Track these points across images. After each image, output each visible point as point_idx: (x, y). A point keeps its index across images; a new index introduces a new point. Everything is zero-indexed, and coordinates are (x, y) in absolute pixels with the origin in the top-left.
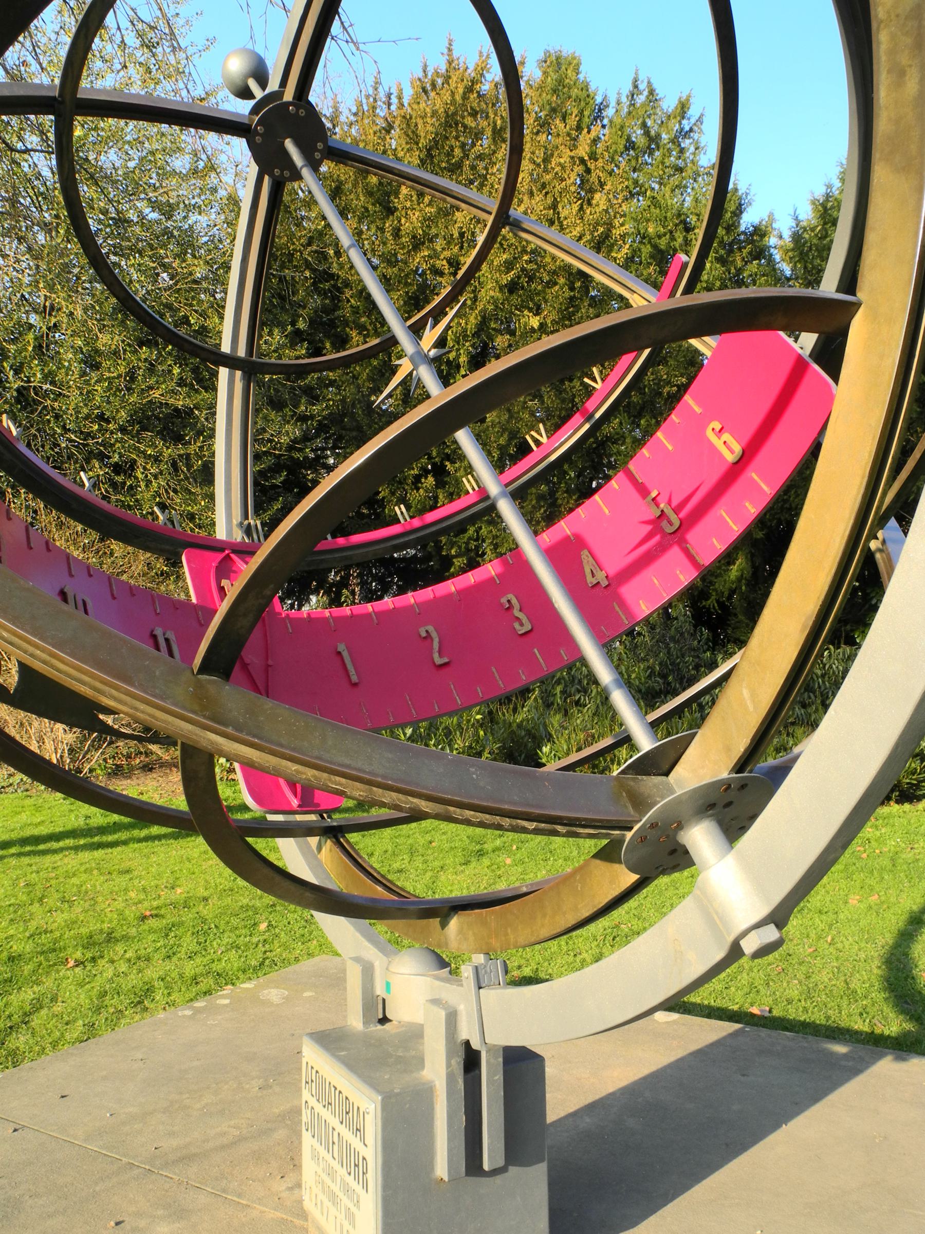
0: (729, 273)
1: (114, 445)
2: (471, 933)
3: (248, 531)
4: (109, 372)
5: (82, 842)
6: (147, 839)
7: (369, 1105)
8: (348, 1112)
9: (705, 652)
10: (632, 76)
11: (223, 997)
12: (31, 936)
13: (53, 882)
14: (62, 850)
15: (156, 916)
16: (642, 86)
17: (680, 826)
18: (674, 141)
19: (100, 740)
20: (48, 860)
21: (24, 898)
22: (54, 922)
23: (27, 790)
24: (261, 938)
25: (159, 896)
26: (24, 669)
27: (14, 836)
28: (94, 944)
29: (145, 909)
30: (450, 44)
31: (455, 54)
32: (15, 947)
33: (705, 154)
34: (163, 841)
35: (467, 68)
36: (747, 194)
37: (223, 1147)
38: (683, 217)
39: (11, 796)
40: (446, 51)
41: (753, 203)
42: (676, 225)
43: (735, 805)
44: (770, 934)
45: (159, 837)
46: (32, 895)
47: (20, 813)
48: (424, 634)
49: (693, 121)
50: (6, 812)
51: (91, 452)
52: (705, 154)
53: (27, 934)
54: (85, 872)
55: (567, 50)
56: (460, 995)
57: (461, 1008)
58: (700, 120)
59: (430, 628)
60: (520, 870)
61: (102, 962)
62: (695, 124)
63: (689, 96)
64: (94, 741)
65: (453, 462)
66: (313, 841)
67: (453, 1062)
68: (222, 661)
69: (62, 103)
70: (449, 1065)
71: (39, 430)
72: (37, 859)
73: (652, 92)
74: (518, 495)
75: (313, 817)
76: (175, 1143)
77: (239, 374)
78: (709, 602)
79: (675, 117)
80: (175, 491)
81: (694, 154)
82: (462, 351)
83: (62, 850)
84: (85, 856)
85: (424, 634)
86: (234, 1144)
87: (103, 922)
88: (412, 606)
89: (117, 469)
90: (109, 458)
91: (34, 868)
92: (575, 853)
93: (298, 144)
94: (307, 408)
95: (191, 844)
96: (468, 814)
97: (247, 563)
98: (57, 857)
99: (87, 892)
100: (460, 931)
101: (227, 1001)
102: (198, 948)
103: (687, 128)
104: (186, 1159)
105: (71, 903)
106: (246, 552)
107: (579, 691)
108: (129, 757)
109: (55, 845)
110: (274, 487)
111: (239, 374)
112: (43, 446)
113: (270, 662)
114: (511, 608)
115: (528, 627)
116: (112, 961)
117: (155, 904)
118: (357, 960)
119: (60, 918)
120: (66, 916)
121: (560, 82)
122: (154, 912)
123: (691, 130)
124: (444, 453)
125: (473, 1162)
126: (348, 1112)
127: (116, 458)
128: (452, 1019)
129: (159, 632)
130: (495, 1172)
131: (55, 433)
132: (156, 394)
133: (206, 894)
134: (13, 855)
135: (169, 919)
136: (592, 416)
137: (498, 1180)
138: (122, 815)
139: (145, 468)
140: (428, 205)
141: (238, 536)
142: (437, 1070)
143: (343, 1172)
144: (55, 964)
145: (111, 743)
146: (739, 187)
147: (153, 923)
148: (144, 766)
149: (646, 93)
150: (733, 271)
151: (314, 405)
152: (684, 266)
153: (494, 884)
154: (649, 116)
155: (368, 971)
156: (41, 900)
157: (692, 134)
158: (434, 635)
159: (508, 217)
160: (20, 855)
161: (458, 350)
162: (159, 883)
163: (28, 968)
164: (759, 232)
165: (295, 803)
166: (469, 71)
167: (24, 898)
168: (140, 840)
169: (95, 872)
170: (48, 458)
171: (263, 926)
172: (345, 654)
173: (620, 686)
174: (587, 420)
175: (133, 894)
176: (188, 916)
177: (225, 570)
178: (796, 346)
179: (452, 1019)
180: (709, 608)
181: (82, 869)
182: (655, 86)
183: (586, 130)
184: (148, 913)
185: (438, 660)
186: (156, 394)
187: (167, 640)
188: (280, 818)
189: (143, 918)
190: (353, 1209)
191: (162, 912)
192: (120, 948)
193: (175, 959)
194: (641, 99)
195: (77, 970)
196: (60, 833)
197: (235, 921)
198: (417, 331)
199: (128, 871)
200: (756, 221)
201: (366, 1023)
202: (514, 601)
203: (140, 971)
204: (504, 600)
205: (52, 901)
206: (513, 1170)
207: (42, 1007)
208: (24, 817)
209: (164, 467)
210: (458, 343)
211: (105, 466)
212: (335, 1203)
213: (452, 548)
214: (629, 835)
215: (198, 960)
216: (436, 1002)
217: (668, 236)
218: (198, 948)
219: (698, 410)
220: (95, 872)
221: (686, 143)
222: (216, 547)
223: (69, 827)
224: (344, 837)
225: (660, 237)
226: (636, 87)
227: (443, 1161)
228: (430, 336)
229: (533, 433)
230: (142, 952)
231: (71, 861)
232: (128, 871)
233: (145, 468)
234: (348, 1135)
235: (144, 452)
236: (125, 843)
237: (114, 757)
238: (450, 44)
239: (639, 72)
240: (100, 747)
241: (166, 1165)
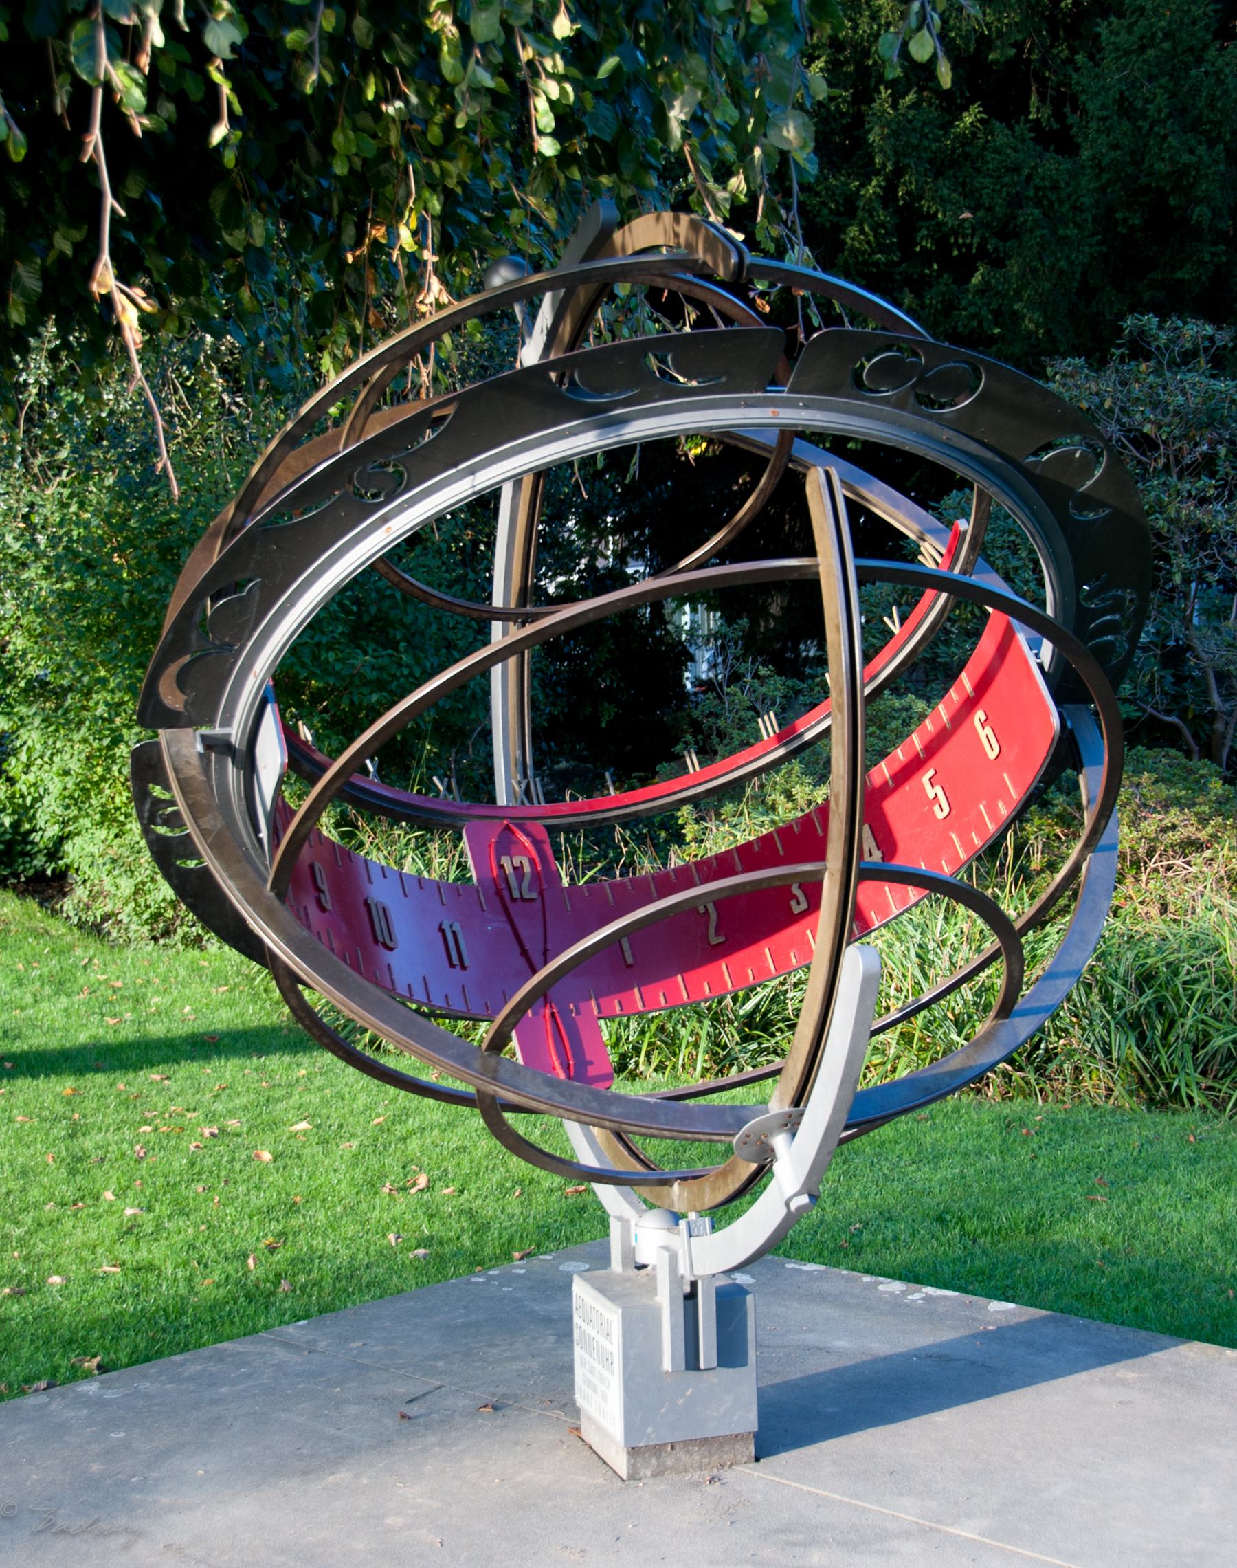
2: (42, 547)
8: (602, 1325)
43: (791, 1124)
44: (804, 1199)
56: (678, 1240)
57: (680, 1253)
118: (619, 1219)
125: (692, 1362)
128: (673, 1259)
129: (446, 926)
138: (707, 1106)
142: (665, 1301)
164: (1199, 223)
179: (673, 1259)
185: (714, 940)
187: (454, 933)
201: (624, 1266)
216: (666, 1248)
224: (463, 877)
227: (668, 1355)
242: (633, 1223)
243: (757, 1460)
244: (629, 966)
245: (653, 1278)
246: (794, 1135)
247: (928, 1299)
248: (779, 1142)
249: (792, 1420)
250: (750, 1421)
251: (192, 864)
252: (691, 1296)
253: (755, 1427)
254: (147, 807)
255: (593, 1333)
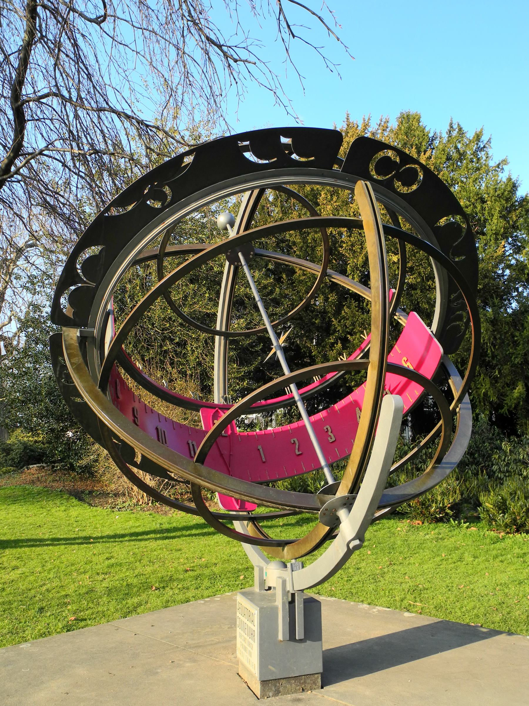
0: (509, 224)
1: (176, 333)
3: (226, 399)
4: (175, 297)
5: (158, 536)
6: (189, 535)
7: (255, 611)
8: (250, 616)
9: (497, 440)
10: (450, 121)
11: (217, 597)
12: (136, 576)
13: (145, 553)
14: (149, 539)
15: (192, 570)
16: (455, 126)
17: (336, 511)
18: (475, 154)
19: (167, 485)
20: (143, 543)
21: (133, 559)
22: (146, 570)
23: (132, 510)
24: (240, 583)
25: (194, 562)
26: (143, 456)
27: (127, 532)
28: (164, 581)
29: (187, 567)
30: (348, 116)
31: (351, 120)
32: (129, 580)
33: (492, 160)
34: (197, 537)
35: (358, 126)
36: (517, 181)
37: (211, 644)
38: (480, 196)
39: (124, 513)
40: (345, 120)
41: (521, 185)
42: (476, 200)
43: (348, 503)
44: (357, 542)
45: (195, 535)
46: (136, 558)
47: (129, 521)
48: (293, 442)
49: (485, 142)
50: (122, 520)
51: (165, 337)
52: (492, 160)
53: (134, 575)
54: (160, 549)
55: (413, 111)
56: (286, 574)
57: (287, 579)
58: (489, 141)
59: (295, 439)
60: (374, 557)
61: (167, 589)
62: (486, 144)
63: (482, 129)
64: (164, 485)
65: (351, 335)
66: (245, 522)
67: (285, 598)
68: (201, 459)
69: (160, 255)
70: (283, 599)
71: (141, 327)
72: (138, 543)
73: (460, 129)
74: (304, 399)
75: (245, 513)
76: (194, 642)
77: (223, 337)
78: (503, 410)
79: (473, 142)
80: (206, 355)
81: (486, 160)
82: (355, 276)
83: (149, 539)
84: (160, 542)
85: (293, 442)
86: (216, 643)
87: (168, 572)
88: (289, 430)
89: (178, 344)
90: (174, 340)
91: (136, 546)
92: (406, 550)
93: (243, 255)
94: (273, 310)
95: (210, 539)
96: (269, 504)
97: (224, 413)
98: (147, 542)
99: (161, 559)
100: (288, 552)
101: (219, 599)
102: (211, 585)
103: (482, 146)
104: (198, 646)
105: (153, 563)
106: (225, 408)
107: (421, 462)
108: (181, 494)
109: (146, 537)
110: (256, 351)
111: (223, 337)
112: (142, 334)
113: (231, 453)
114: (327, 431)
115: (334, 439)
116: (172, 589)
117: (192, 565)
118: (258, 566)
119: (149, 569)
120: (151, 568)
121: (409, 128)
122: (191, 569)
123: (484, 147)
124: (346, 332)
125: (292, 636)
126: (250, 616)
127: (177, 340)
128: (284, 583)
129: (190, 442)
130: (301, 641)
131: (148, 328)
132: (197, 307)
133: (216, 562)
134: (126, 541)
135: (198, 572)
136: (364, 350)
137: (303, 645)
139: (191, 345)
140: (335, 202)
141: (222, 402)
142: (279, 602)
143: (248, 638)
144: (147, 589)
145: (173, 486)
146: (512, 177)
147: (191, 573)
148: (189, 499)
149: (457, 130)
150: (511, 222)
151: (277, 308)
152: (394, 294)
153: (359, 563)
154: (460, 142)
155: (261, 570)
156: (140, 561)
157: (485, 149)
158: (297, 442)
159: (326, 273)
160: (129, 541)
161: (353, 275)
162: (194, 556)
163: (135, 590)
165: (238, 507)
166: (359, 128)
167: (133, 559)
168: (186, 536)
169: (165, 550)
170: (145, 340)
171: (242, 577)
172: (261, 450)
173: (327, 467)
174: (362, 352)
175: (182, 560)
176: (207, 572)
177: (216, 416)
178: (429, 331)
179: (284, 583)
180: (503, 414)
181: (159, 548)
182: (462, 126)
183: (423, 153)
184: (188, 569)
185: (297, 453)
186: (197, 307)
187: (193, 445)
188: (234, 513)
189: (187, 571)
190: (251, 650)
191: (195, 569)
192: (175, 584)
193: (200, 589)
194: (455, 133)
195: (156, 591)
196: (148, 531)
197: (229, 575)
198: (278, 335)
199: (180, 550)
200: (524, 195)
201: (260, 589)
202: (329, 428)
203: (184, 593)
204: (325, 428)
205: (145, 561)
206: (308, 642)
207: (141, 605)
208: (131, 523)
209: (200, 344)
210: (354, 272)
211: (172, 344)
212: (246, 650)
213: (352, 382)
214: (319, 512)
215: (210, 590)
217: (471, 206)
218: (211, 585)
219: (399, 352)
220: (165, 550)
221: (482, 154)
222: (213, 406)
223: (152, 529)
225: (467, 207)
226: (452, 127)
228: (283, 338)
229: (341, 357)
230: (185, 585)
231: (153, 544)
232: (180, 550)
233: (191, 345)
234: (249, 623)
235: (191, 336)
236: (179, 537)
237: (174, 494)
238: (348, 116)
239: (453, 119)
240: (167, 489)
241: (190, 648)
242: (264, 568)
243: (322, 688)
244: (264, 462)
245: (274, 595)
246: (350, 511)
247: (379, 611)
248: (342, 513)
249: (340, 666)
250: (320, 668)
251: (78, 400)
252: (292, 603)
253: (321, 670)
254: (58, 369)
255: (245, 621)
